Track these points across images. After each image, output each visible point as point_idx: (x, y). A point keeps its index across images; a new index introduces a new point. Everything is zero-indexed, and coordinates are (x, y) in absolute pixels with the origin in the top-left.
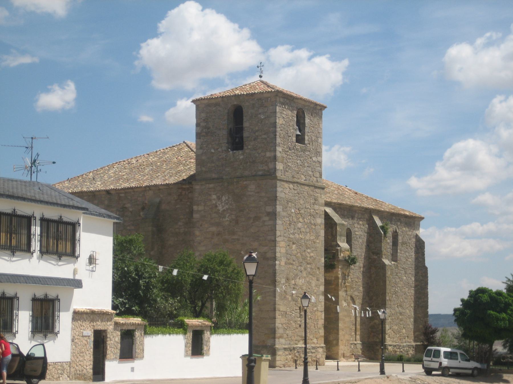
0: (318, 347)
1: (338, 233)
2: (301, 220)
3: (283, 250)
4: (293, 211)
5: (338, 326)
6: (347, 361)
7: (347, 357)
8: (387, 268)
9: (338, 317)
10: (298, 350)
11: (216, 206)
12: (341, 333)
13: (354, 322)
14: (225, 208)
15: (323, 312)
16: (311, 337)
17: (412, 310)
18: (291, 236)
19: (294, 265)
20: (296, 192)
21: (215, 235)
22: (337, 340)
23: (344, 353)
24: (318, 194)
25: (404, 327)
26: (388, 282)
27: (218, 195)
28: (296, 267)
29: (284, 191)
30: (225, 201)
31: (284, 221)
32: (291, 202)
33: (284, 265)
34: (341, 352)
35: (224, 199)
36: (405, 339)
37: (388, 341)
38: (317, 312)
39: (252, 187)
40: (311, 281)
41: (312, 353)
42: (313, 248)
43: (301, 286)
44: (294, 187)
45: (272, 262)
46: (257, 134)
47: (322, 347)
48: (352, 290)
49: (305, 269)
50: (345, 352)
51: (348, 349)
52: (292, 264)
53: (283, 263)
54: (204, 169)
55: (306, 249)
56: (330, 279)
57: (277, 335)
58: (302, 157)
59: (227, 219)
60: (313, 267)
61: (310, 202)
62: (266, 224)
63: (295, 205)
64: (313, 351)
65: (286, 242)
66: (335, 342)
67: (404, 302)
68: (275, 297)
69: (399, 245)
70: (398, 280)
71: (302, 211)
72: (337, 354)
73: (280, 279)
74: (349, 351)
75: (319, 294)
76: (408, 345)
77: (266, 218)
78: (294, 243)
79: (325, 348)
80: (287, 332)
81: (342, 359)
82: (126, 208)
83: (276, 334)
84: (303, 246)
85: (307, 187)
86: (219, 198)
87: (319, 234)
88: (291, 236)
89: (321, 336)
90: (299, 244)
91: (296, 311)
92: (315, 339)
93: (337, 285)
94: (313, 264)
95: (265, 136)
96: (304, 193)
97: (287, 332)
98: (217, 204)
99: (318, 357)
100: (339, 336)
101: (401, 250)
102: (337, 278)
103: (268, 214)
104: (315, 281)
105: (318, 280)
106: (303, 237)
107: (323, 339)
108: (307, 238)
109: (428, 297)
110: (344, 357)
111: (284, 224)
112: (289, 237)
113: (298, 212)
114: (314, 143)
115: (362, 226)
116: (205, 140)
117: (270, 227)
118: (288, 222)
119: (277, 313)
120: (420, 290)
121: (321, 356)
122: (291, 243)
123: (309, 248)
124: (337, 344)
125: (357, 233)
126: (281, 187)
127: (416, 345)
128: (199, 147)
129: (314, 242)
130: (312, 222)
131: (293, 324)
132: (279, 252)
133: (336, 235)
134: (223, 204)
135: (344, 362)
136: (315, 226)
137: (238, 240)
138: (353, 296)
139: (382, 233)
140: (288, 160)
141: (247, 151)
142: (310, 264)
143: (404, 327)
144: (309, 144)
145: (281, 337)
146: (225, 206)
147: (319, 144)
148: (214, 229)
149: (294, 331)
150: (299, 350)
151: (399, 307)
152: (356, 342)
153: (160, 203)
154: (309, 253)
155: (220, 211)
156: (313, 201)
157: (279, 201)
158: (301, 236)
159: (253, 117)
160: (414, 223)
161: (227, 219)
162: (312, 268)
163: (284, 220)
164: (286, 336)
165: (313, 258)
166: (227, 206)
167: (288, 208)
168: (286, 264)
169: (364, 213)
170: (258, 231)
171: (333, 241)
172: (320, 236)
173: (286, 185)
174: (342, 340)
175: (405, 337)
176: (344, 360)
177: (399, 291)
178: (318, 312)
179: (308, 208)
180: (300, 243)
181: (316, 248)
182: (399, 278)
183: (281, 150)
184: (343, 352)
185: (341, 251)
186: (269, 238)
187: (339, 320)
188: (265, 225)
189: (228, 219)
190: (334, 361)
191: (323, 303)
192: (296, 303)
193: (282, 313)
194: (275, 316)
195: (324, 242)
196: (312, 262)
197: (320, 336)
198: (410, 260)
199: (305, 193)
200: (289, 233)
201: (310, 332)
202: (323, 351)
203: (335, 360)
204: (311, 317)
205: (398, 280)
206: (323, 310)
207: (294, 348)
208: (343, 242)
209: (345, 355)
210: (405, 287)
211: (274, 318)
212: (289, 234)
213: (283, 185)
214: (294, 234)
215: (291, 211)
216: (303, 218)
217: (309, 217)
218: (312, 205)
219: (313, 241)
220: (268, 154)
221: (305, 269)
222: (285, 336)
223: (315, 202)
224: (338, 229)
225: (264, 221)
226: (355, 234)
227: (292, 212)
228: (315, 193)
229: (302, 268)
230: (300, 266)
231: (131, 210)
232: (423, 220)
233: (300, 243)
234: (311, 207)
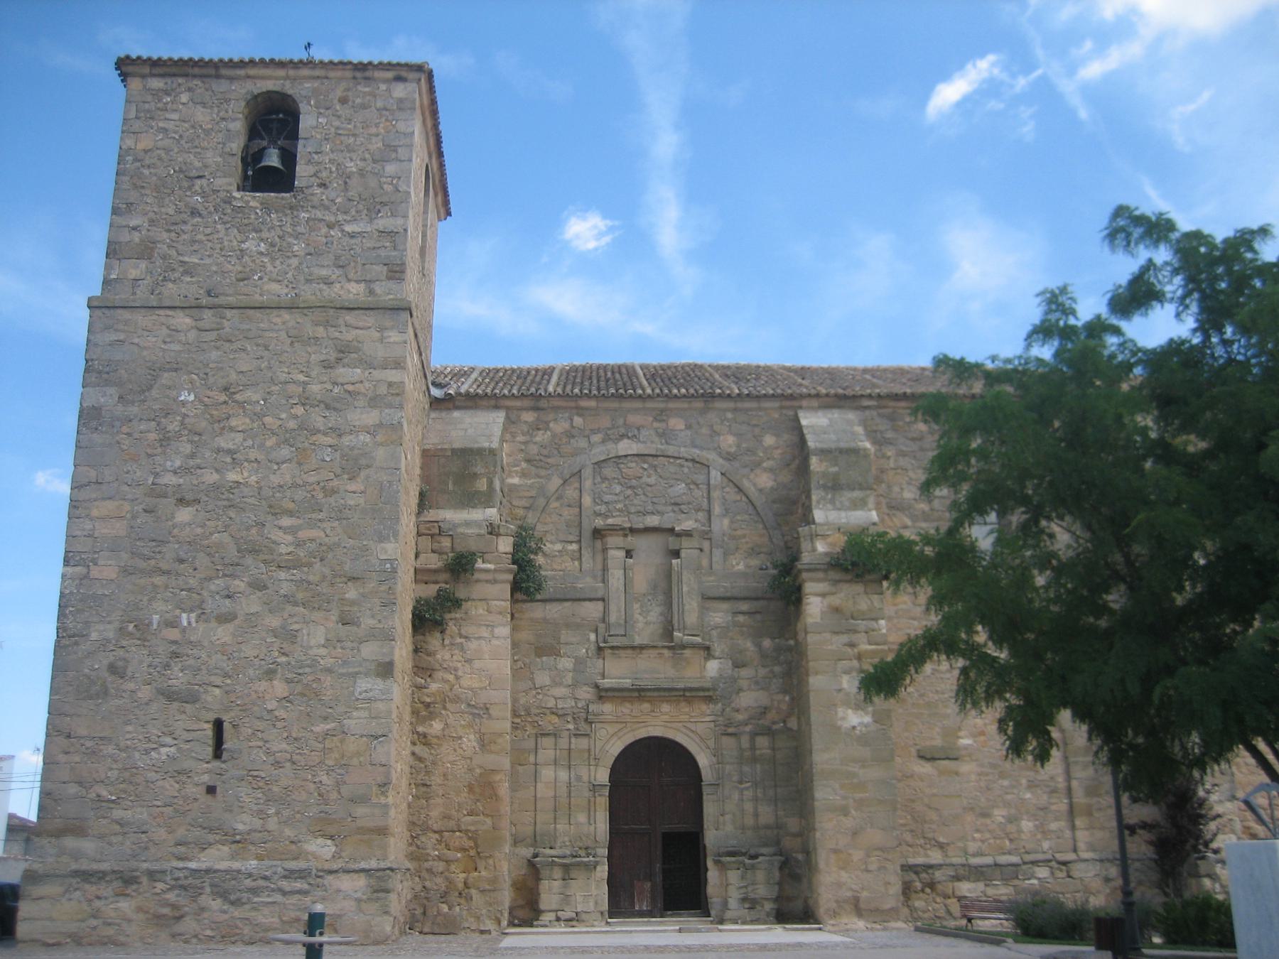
41: (284, 893)
203: (787, 926)
209: (862, 905)
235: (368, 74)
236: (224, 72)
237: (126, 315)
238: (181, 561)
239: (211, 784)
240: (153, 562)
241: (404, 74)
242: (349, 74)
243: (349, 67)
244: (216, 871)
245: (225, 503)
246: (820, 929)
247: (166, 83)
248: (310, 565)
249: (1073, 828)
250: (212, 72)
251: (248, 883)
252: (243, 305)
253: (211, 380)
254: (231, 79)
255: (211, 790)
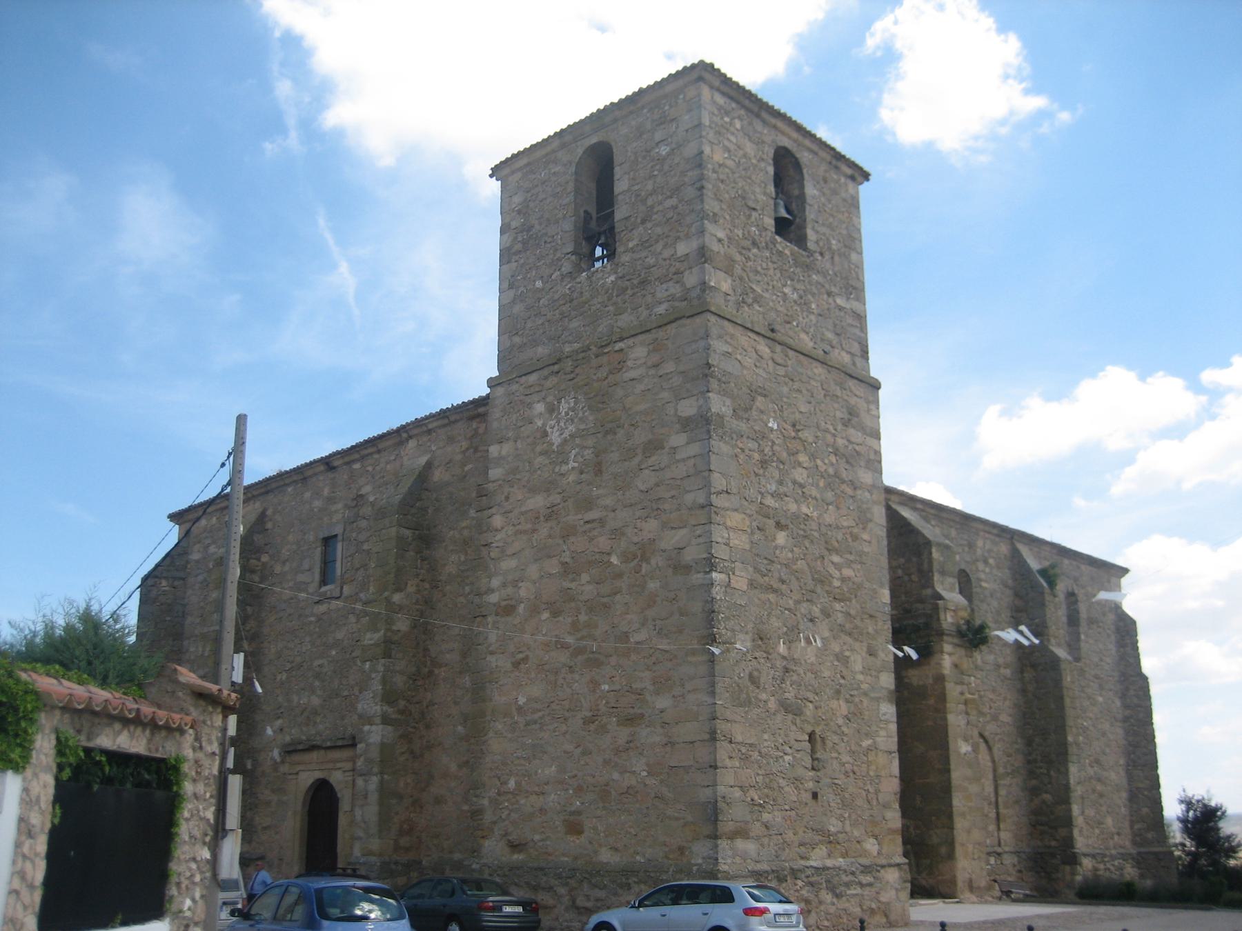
0: (883, 867)
1: (936, 566)
2: (803, 458)
3: (740, 541)
4: (772, 424)
5: (951, 806)
6: (981, 903)
7: (979, 888)
8: (1063, 666)
9: (950, 783)
10: (807, 877)
11: (545, 434)
12: (960, 824)
13: (993, 800)
14: (566, 434)
15: (896, 755)
16: (856, 833)
17: (1123, 773)
18: (769, 501)
19: (782, 594)
20: (781, 371)
21: (542, 518)
22: (951, 844)
23: (971, 881)
24: (858, 400)
25: (1108, 812)
26: (1067, 701)
27: (550, 399)
28: (791, 602)
29: (739, 357)
30: (567, 414)
31: (743, 450)
32: (765, 396)
33: (745, 588)
34: (961, 877)
35: (564, 407)
36: (1112, 839)
37: (1082, 841)
38: (873, 753)
39: (639, 352)
40: (847, 653)
41: (862, 885)
42: (851, 553)
43: (812, 664)
44: (775, 356)
45: (700, 575)
46: (650, 202)
47: (898, 865)
48: (981, 720)
49: (826, 614)
50: (974, 876)
51: (982, 869)
52: (775, 591)
53: (740, 582)
54: (517, 340)
55: (826, 553)
56: (921, 683)
57: (726, 826)
58: (799, 281)
59: (572, 464)
60: (853, 612)
61: (832, 414)
62: (678, 457)
63: (781, 411)
64: (867, 879)
65: (750, 516)
66: (943, 850)
67: (1104, 753)
68: (713, 693)
69: (1083, 623)
70: (1086, 703)
71: (807, 435)
72: (953, 882)
73: (729, 633)
74: (985, 873)
75: (880, 698)
76: (1122, 854)
77: (678, 440)
78: (779, 526)
79: (906, 867)
80: (766, 816)
81: (967, 895)
82: (362, 496)
83: (720, 824)
84: (815, 540)
85: (820, 370)
86: (552, 409)
87: (869, 515)
88: (769, 501)
89: (892, 831)
90: (802, 533)
91: (797, 746)
92: (872, 840)
93: (942, 698)
94: (854, 601)
95: (673, 201)
96: (809, 383)
97: (766, 816)
98: (548, 428)
99: (884, 898)
100: (955, 832)
101: (1087, 636)
102: (940, 679)
103: (686, 424)
104: (864, 654)
105: (872, 653)
106: (815, 514)
107: (899, 840)
108: (829, 518)
109: (1155, 743)
110: (971, 887)
111: (742, 457)
112: (761, 503)
113: (793, 434)
114: (836, 258)
115: (995, 571)
116: (522, 261)
117: (692, 462)
118: (756, 456)
119: (723, 751)
120: (1135, 728)
121: (894, 897)
122: (771, 522)
123: (837, 552)
124: (951, 856)
125: (984, 584)
126: (726, 341)
127: (1139, 853)
128: (506, 285)
129: (855, 538)
130: (844, 474)
131: (787, 789)
132: (726, 544)
133: (931, 570)
134: (562, 424)
135: (974, 903)
136: (855, 489)
137: (602, 522)
138: (986, 734)
139: (1045, 584)
140: (751, 275)
141: (625, 258)
142: (840, 600)
143: (1108, 812)
144: (821, 254)
145: (742, 833)
146: (567, 428)
147: (853, 267)
148: (538, 502)
149: (793, 813)
150: (812, 879)
151: (1095, 765)
152: (999, 850)
153: (429, 465)
154: (838, 567)
155: (555, 447)
156: (842, 416)
157: (719, 380)
158: (804, 509)
159: (640, 160)
160: (1109, 581)
161: (572, 464)
162: (850, 615)
163: (741, 445)
164: (764, 829)
165: (851, 584)
166: (572, 428)
167: (754, 413)
168: (752, 584)
169: (997, 539)
170: (657, 485)
171: (924, 587)
172: (871, 521)
173: (744, 339)
174: (963, 845)
175: (1113, 835)
176: (974, 898)
177: (1091, 728)
178: (876, 755)
179: (827, 431)
180: (804, 530)
181: (860, 556)
182: (1089, 698)
183: (721, 235)
184: (968, 876)
185: (946, 609)
186: (689, 498)
187: (953, 790)
188: (678, 461)
189: (576, 465)
190: (944, 902)
191: (893, 727)
192: (798, 718)
193: (744, 751)
194: (715, 760)
195: (885, 543)
196: (847, 595)
197: (889, 829)
198: (1108, 660)
199: (814, 383)
200: (763, 490)
201: (854, 817)
202: (901, 877)
203: (947, 900)
204: (855, 768)
205: (1086, 703)
206: (895, 747)
207: (795, 873)
208: (951, 590)
209: (975, 885)
210: (1102, 720)
211: (711, 766)
212: (762, 494)
213: (732, 336)
214: (776, 495)
215: (766, 425)
216: (813, 457)
217: (833, 458)
218: (840, 427)
219: (851, 533)
220: (682, 248)
221: (826, 614)
222: (757, 829)
223: (849, 420)
224: (936, 554)
225: (674, 450)
226: (981, 586)
227: (772, 430)
228: (849, 393)
229: (816, 611)
230: (808, 600)
231: (372, 499)
232: (1127, 576)
233: (804, 530)
234: (835, 430)
235: (839, 164)
236: (764, 115)
237: (738, 332)
238: (783, 582)
239: (814, 790)
240: (766, 579)
241: (857, 175)
242: (828, 158)
243: (832, 152)
244: (828, 868)
245: (802, 533)
246: (958, 902)
247: (725, 103)
248: (850, 600)
249: (999, 829)
250: (756, 109)
251: (845, 878)
252: (799, 349)
253: (785, 414)
254: (764, 122)
255: (815, 796)
